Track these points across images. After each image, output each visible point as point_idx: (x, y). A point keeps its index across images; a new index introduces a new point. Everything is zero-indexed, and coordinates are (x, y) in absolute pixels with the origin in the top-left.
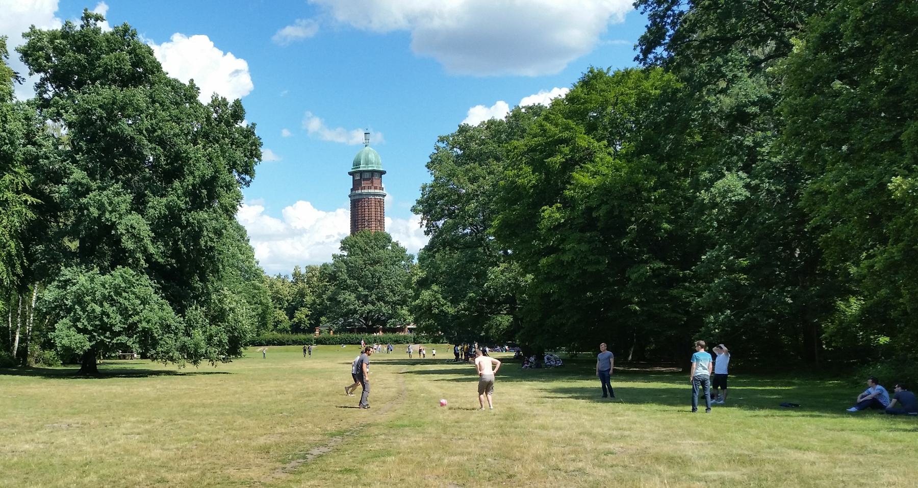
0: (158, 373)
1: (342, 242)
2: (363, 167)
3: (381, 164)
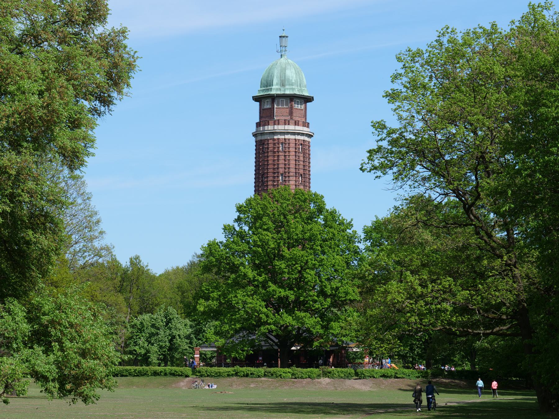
1: (240, 209)
2: (277, 89)
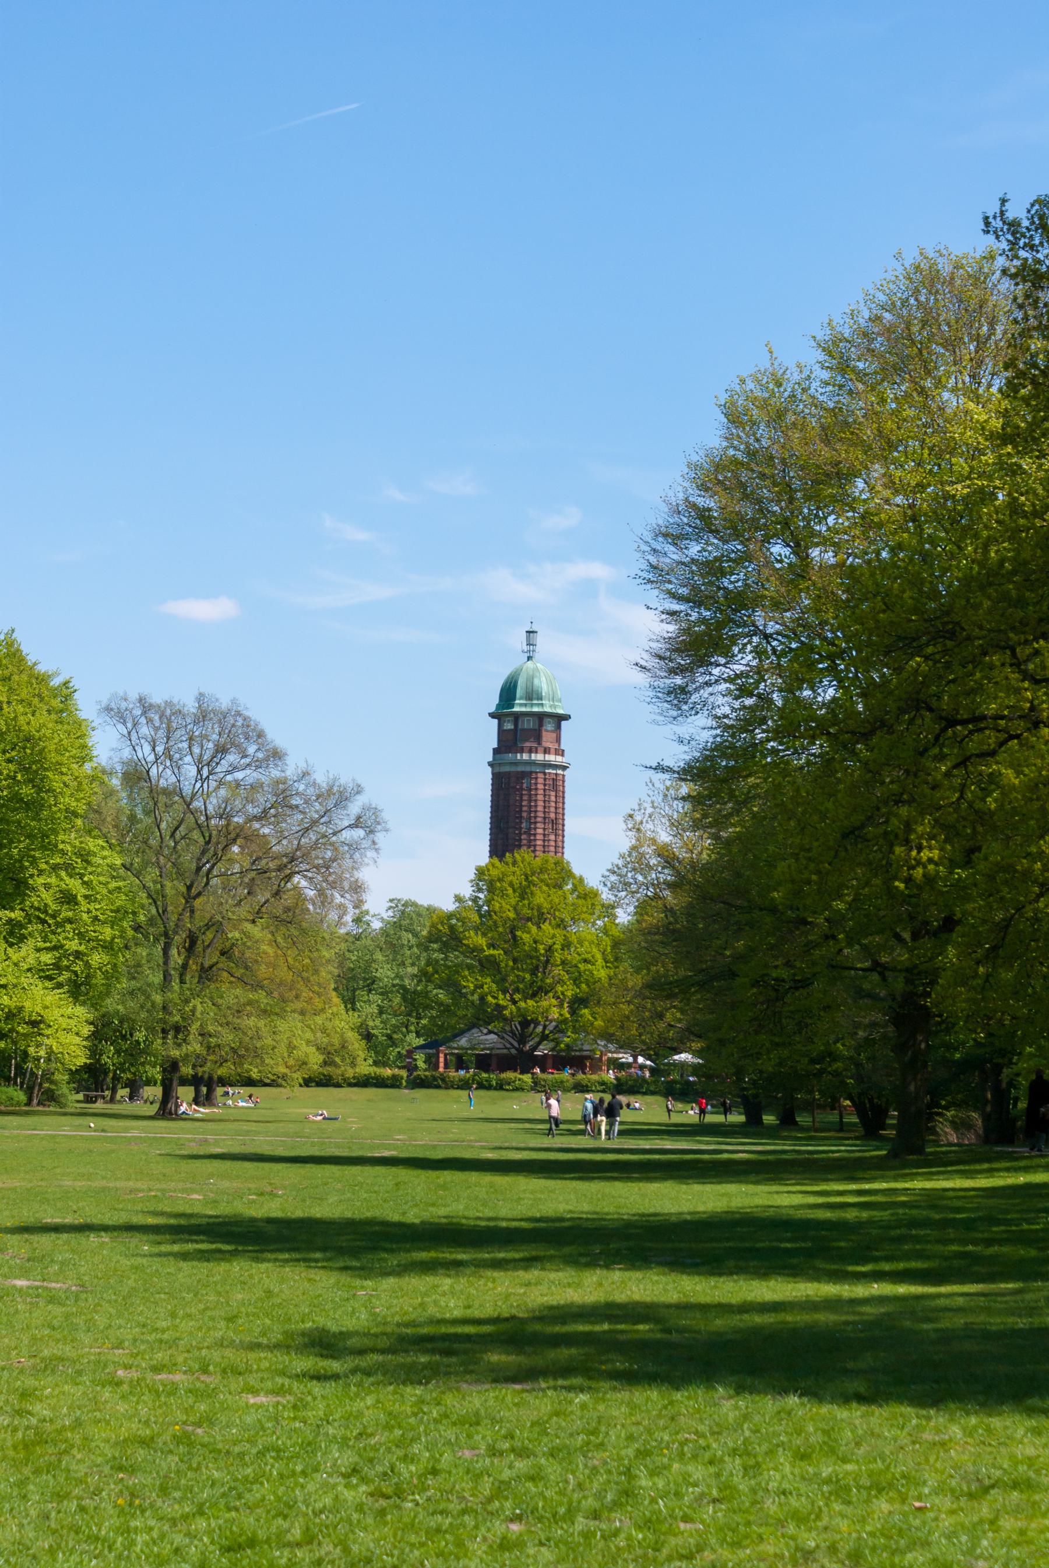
0: (521, 1220)
2: (521, 705)
3: (560, 701)
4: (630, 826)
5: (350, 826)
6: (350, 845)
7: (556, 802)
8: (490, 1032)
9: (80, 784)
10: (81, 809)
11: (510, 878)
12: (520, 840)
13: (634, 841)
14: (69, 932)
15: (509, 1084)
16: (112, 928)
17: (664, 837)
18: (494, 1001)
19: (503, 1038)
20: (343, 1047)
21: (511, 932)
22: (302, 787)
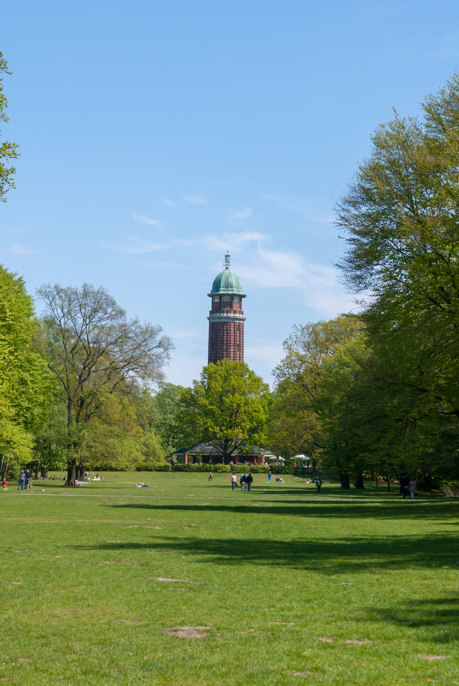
2: (223, 290)
4: (286, 347)
5: (156, 347)
6: (156, 356)
7: (240, 336)
8: (210, 445)
9: (29, 327)
10: (29, 339)
11: (220, 372)
12: (223, 354)
13: (288, 354)
14: (23, 398)
15: (220, 469)
16: (44, 396)
17: (302, 352)
18: (213, 430)
19: (216, 448)
20: (154, 452)
21: (220, 397)
22: (134, 328)
